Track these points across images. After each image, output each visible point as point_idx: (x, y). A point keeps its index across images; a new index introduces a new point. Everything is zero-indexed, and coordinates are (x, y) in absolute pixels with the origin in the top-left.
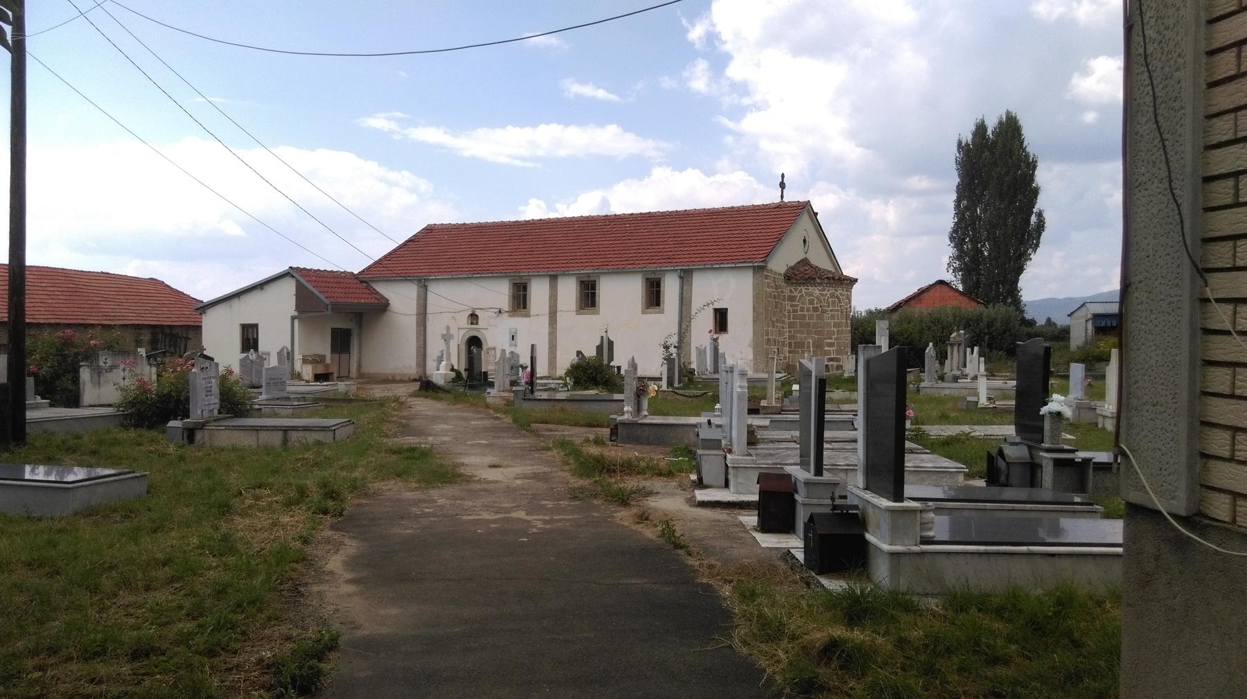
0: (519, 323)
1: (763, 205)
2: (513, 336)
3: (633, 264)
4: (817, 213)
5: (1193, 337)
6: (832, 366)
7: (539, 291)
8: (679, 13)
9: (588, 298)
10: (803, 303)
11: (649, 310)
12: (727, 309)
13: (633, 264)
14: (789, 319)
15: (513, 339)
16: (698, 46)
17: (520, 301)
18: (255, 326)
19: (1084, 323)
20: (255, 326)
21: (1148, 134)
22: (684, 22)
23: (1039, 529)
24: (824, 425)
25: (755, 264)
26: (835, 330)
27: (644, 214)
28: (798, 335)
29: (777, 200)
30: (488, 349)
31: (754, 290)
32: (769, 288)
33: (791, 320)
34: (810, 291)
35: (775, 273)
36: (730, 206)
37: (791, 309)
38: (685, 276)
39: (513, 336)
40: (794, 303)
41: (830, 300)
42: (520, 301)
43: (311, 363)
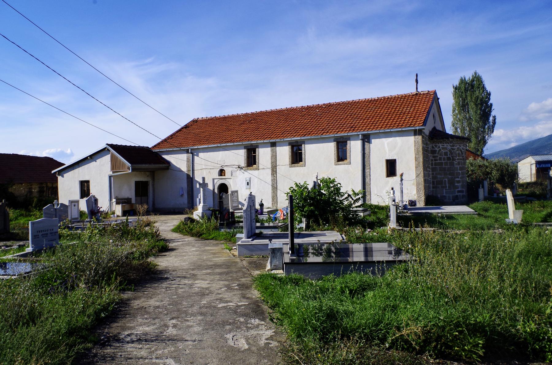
0: (251, 173)
2: (248, 183)
4: (439, 98)
6: (460, 195)
10: (441, 155)
11: (340, 162)
12: (395, 160)
14: (432, 165)
15: (248, 185)
18: (88, 182)
19: (530, 166)
20: (88, 182)
26: (460, 172)
28: (439, 176)
29: (414, 91)
30: (232, 192)
33: (434, 166)
34: (445, 146)
37: (433, 159)
38: (366, 139)
39: (248, 183)
40: (436, 155)
41: (457, 152)
43: (122, 203)
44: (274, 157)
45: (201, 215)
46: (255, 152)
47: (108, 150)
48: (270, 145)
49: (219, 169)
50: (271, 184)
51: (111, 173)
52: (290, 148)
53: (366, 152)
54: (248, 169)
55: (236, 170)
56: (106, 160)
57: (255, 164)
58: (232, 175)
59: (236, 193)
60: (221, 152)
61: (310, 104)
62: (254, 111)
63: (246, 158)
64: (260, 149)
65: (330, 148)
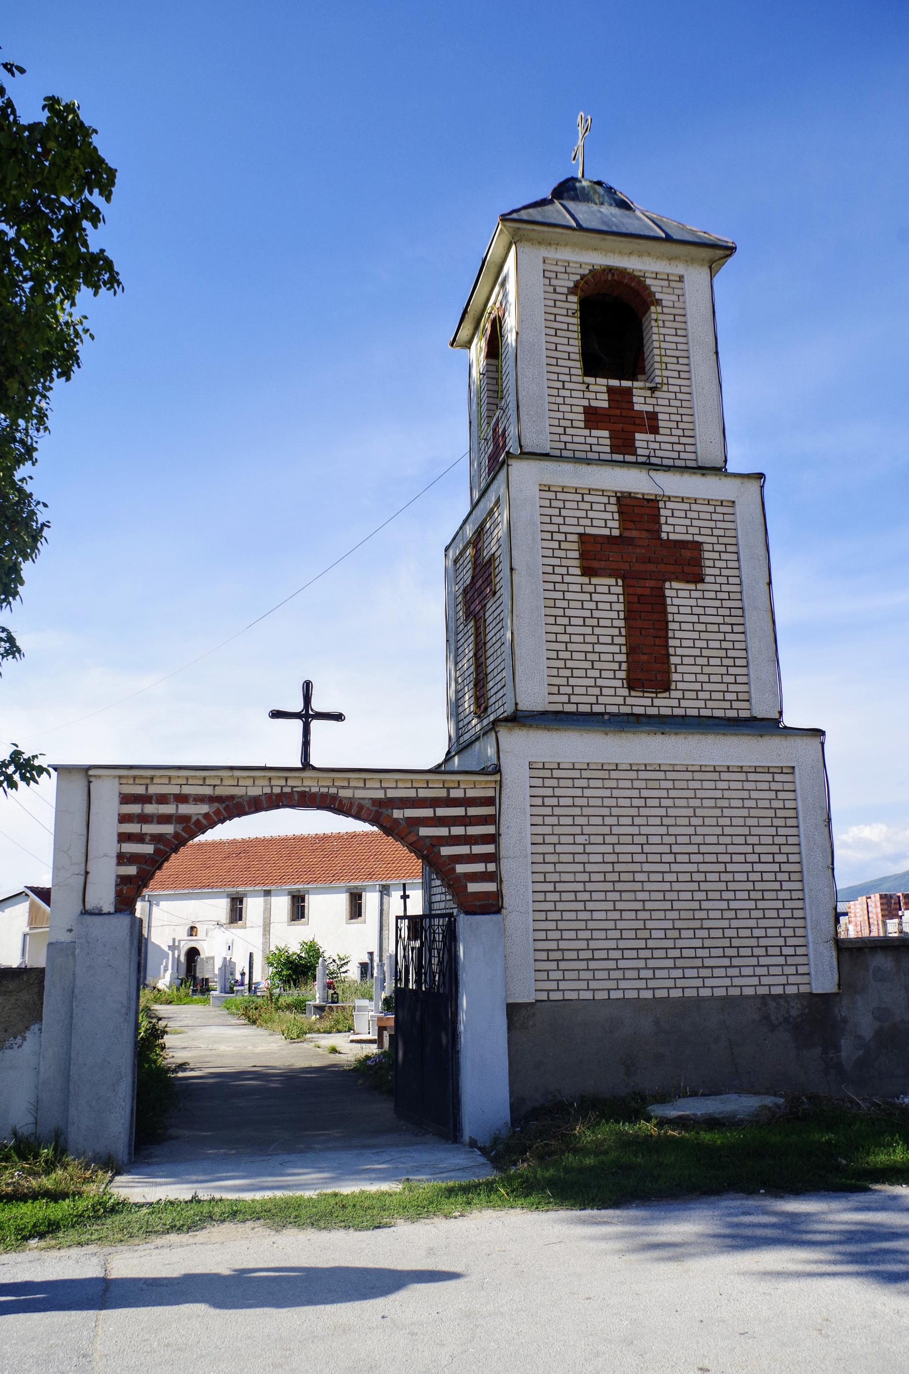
0: (235, 933)
5: (565, 261)
7: (253, 906)
9: (298, 911)
11: (353, 921)
17: (236, 914)
21: (836, 1099)
42: (236, 914)
44: (268, 911)
45: (168, 984)
46: (241, 902)
47: (27, 895)
48: (262, 893)
49: (189, 926)
50: (261, 949)
51: (27, 930)
52: (348, 897)
53: (385, 907)
54: (230, 928)
55: (214, 927)
56: (21, 910)
57: (241, 919)
58: (207, 935)
59: (212, 960)
60: (193, 902)
61: (328, 832)
62: (245, 837)
63: (229, 910)
64: (249, 899)
65: (341, 901)
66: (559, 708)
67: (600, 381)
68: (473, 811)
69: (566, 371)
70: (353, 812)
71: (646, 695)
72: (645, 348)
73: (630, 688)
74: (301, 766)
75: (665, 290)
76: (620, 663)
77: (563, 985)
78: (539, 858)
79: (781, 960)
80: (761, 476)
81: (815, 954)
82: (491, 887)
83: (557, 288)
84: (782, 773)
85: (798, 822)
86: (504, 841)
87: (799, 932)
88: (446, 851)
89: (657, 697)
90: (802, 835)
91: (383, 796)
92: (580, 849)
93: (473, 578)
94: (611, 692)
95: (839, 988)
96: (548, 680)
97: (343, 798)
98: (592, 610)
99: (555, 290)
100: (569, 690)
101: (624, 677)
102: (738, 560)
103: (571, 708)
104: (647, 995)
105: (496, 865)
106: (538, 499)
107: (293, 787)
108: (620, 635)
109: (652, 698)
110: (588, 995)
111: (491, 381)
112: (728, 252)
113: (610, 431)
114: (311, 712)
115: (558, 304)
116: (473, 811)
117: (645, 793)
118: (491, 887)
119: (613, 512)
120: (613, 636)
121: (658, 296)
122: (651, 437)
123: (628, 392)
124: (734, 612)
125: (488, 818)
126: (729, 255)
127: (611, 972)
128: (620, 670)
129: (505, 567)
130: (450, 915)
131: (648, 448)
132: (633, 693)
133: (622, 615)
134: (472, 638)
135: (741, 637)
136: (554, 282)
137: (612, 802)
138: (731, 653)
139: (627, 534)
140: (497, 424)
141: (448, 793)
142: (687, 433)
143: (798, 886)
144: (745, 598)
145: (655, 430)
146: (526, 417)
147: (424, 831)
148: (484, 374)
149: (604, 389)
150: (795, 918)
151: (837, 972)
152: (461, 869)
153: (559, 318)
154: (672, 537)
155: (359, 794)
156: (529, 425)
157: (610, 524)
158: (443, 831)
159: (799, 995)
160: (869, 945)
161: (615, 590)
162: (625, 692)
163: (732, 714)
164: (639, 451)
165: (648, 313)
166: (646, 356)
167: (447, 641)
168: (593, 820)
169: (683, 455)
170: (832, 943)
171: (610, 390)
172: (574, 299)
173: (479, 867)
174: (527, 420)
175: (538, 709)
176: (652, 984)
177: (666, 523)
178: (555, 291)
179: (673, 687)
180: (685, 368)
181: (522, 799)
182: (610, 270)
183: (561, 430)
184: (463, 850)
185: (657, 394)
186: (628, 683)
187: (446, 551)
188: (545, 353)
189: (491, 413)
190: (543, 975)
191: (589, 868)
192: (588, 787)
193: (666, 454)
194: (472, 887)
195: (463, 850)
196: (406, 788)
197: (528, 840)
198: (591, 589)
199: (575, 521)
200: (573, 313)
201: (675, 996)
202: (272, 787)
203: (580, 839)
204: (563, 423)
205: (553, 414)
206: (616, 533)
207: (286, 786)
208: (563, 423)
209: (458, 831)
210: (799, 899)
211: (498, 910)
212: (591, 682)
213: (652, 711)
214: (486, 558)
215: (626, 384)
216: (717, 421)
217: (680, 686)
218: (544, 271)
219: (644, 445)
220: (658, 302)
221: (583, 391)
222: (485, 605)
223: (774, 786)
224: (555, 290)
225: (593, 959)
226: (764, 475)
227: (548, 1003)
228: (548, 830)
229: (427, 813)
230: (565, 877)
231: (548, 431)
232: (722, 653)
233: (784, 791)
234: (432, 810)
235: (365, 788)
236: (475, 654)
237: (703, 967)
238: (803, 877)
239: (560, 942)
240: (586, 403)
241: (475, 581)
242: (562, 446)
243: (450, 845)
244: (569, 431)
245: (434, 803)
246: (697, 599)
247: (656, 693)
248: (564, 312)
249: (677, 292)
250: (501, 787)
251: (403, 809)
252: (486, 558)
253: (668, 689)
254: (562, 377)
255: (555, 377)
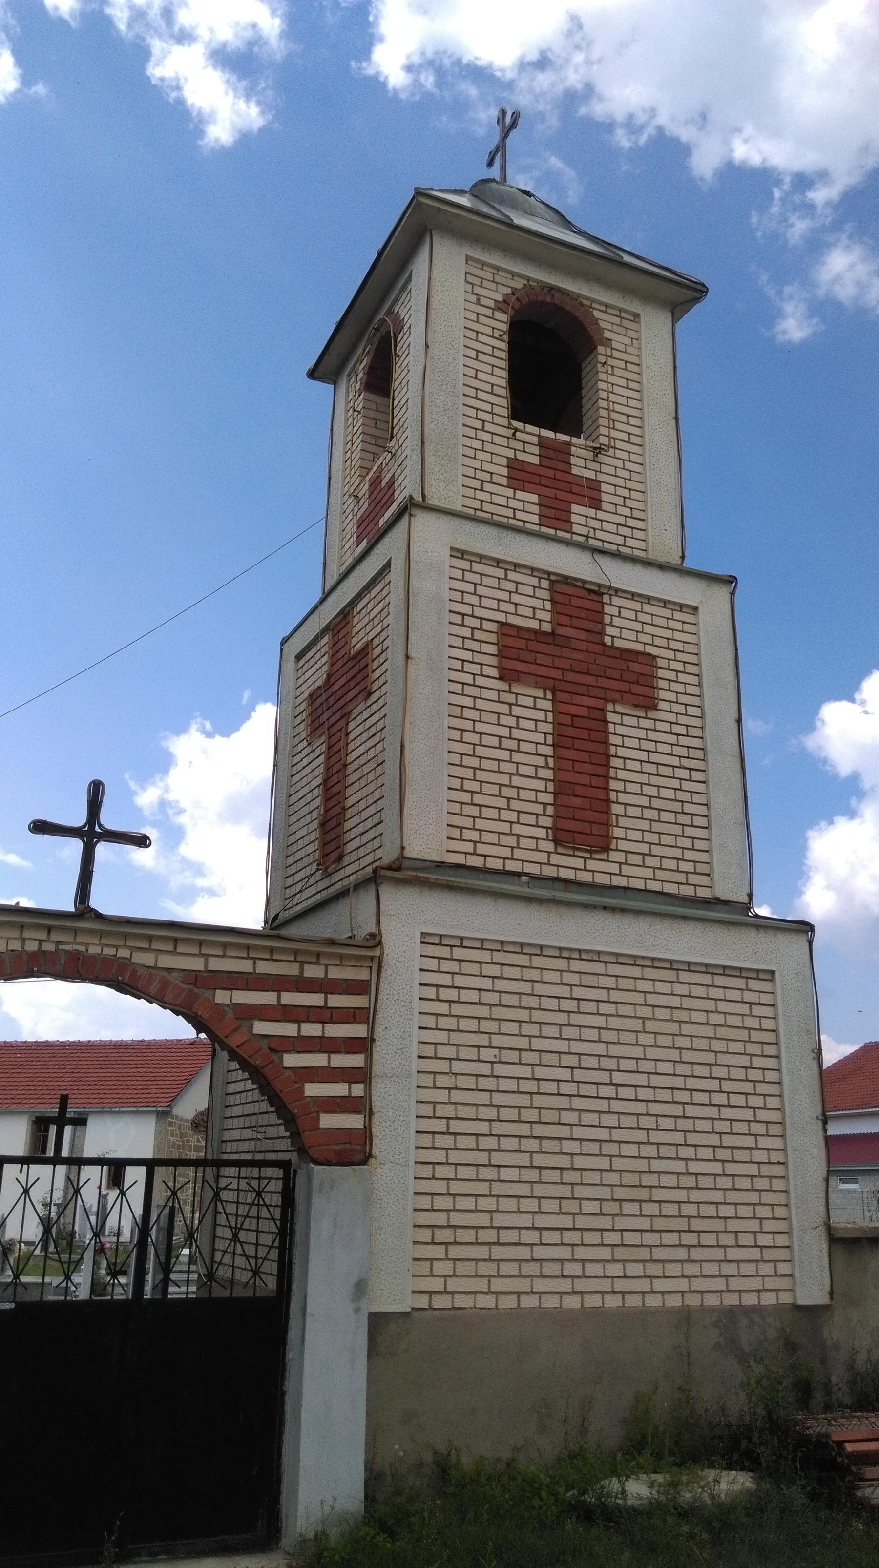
1: (177, 1040)
3: (19, 1103)
5: (788, 1175)
8: (127, 776)
13: (19, 1103)
16: (147, 812)
22: (133, 785)
23: (859, 1494)
24: (237, 1298)
25: (159, 1109)
27: (40, 1042)
31: (156, 1138)
32: (172, 1136)
35: (181, 1120)
36: (140, 1038)
66: (460, 859)
67: (530, 428)
68: (337, 1001)
69: (488, 407)
70: (153, 990)
71: (577, 853)
72: (584, 401)
73: (557, 842)
74: (72, 909)
75: (616, 328)
76: (545, 805)
77: (453, 1284)
78: (428, 1080)
79: (755, 1254)
80: (731, 580)
81: (800, 1246)
82: (355, 1121)
83: (482, 298)
84: (758, 979)
85: (779, 1050)
86: (379, 1050)
87: (780, 1212)
88: (291, 1060)
89: (591, 858)
90: (784, 1070)
91: (202, 968)
92: (485, 1069)
93: (329, 676)
94: (531, 844)
95: (831, 1299)
96: (447, 819)
97: (138, 964)
98: (510, 727)
99: (478, 300)
100: (474, 836)
101: (550, 825)
102: (700, 685)
103: (475, 862)
104: (572, 1303)
105: (366, 1086)
106: (447, 567)
107: (58, 943)
108: (547, 766)
109: (585, 858)
110: (487, 1302)
111: (368, 422)
112: (697, 295)
113: (539, 495)
114: (97, 829)
115: (482, 319)
116: (337, 1001)
117: (578, 992)
118: (355, 1121)
119: (544, 600)
120: (537, 767)
121: (607, 334)
122: (592, 512)
123: (564, 451)
124: (693, 753)
125: (357, 1012)
126: (697, 300)
127: (524, 1265)
128: (544, 815)
129: (395, 656)
130: (285, 1165)
131: (586, 526)
132: (560, 850)
133: (550, 740)
134: (322, 759)
135: (701, 788)
136: (478, 290)
137: (533, 1002)
138: (689, 808)
139: (561, 631)
140: (380, 469)
141: (302, 970)
142: (636, 514)
143: (777, 1143)
144: (708, 736)
145: (596, 503)
146: (433, 458)
147: (261, 1027)
148: (359, 412)
149: (535, 440)
150: (775, 1191)
151: (828, 1273)
152: (312, 1090)
153: (482, 338)
154: (618, 643)
155: (166, 961)
156: (436, 469)
157: (540, 615)
158: (289, 1029)
159: (779, 1308)
160: (869, 1235)
161: (541, 704)
162: (550, 846)
163: (688, 891)
164: (576, 528)
165: (593, 355)
166: (584, 410)
167: (275, 766)
168: (506, 1027)
169: (630, 542)
170: (822, 1230)
171: (542, 443)
172: (504, 317)
173: (339, 1089)
174: (433, 463)
175: (432, 859)
176: (580, 1285)
177: (611, 624)
178: (478, 302)
179: (613, 846)
180: (637, 431)
181: (408, 987)
182: (552, 288)
183: (477, 484)
184: (317, 1060)
185: (601, 458)
186: (554, 835)
187: (282, 644)
188: (461, 379)
189: (367, 464)
190: (424, 1268)
191: (498, 1099)
192: (502, 977)
193: (609, 538)
194: (328, 1121)
195: (317, 1060)
196: (238, 957)
197: (415, 1050)
198: (511, 698)
199: (494, 604)
200: (500, 335)
201: (571, 1306)
202: (24, 940)
203: (488, 1054)
204: (480, 475)
205: (468, 461)
206: (547, 627)
207: (48, 940)
208: (480, 475)
209: (311, 1029)
210: (779, 1163)
211: (365, 1159)
212: (504, 827)
213: (585, 877)
214: (357, 647)
215: (562, 437)
216: (674, 503)
217: (622, 845)
218: (466, 273)
219: (582, 520)
220: (608, 342)
221: (508, 438)
222: (350, 713)
223: (749, 997)
224: (478, 300)
225: (497, 1243)
226: (736, 578)
227: (429, 1312)
228: (442, 1037)
229: (267, 998)
230: (463, 1112)
231: (460, 483)
232: (677, 807)
233: (760, 1004)
234: (275, 994)
235: (174, 953)
236: (325, 781)
237: (689, 1261)
238: (784, 1130)
239: (452, 1214)
240: (511, 454)
241: (332, 680)
242: (477, 505)
243: (299, 1052)
244: (487, 487)
245: (279, 984)
246: (647, 729)
247: (591, 852)
248: (489, 331)
249: (631, 333)
250: (380, 967)
251: (231, 989)
252: (357, 647)
253: (606, 849)
254: (482, 415)
255: (472, 413)
